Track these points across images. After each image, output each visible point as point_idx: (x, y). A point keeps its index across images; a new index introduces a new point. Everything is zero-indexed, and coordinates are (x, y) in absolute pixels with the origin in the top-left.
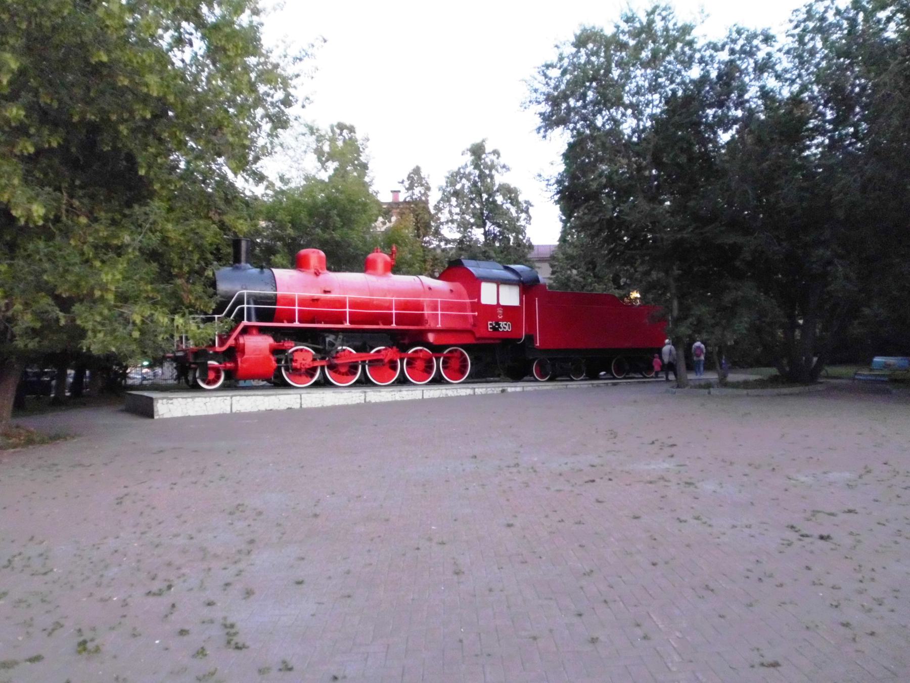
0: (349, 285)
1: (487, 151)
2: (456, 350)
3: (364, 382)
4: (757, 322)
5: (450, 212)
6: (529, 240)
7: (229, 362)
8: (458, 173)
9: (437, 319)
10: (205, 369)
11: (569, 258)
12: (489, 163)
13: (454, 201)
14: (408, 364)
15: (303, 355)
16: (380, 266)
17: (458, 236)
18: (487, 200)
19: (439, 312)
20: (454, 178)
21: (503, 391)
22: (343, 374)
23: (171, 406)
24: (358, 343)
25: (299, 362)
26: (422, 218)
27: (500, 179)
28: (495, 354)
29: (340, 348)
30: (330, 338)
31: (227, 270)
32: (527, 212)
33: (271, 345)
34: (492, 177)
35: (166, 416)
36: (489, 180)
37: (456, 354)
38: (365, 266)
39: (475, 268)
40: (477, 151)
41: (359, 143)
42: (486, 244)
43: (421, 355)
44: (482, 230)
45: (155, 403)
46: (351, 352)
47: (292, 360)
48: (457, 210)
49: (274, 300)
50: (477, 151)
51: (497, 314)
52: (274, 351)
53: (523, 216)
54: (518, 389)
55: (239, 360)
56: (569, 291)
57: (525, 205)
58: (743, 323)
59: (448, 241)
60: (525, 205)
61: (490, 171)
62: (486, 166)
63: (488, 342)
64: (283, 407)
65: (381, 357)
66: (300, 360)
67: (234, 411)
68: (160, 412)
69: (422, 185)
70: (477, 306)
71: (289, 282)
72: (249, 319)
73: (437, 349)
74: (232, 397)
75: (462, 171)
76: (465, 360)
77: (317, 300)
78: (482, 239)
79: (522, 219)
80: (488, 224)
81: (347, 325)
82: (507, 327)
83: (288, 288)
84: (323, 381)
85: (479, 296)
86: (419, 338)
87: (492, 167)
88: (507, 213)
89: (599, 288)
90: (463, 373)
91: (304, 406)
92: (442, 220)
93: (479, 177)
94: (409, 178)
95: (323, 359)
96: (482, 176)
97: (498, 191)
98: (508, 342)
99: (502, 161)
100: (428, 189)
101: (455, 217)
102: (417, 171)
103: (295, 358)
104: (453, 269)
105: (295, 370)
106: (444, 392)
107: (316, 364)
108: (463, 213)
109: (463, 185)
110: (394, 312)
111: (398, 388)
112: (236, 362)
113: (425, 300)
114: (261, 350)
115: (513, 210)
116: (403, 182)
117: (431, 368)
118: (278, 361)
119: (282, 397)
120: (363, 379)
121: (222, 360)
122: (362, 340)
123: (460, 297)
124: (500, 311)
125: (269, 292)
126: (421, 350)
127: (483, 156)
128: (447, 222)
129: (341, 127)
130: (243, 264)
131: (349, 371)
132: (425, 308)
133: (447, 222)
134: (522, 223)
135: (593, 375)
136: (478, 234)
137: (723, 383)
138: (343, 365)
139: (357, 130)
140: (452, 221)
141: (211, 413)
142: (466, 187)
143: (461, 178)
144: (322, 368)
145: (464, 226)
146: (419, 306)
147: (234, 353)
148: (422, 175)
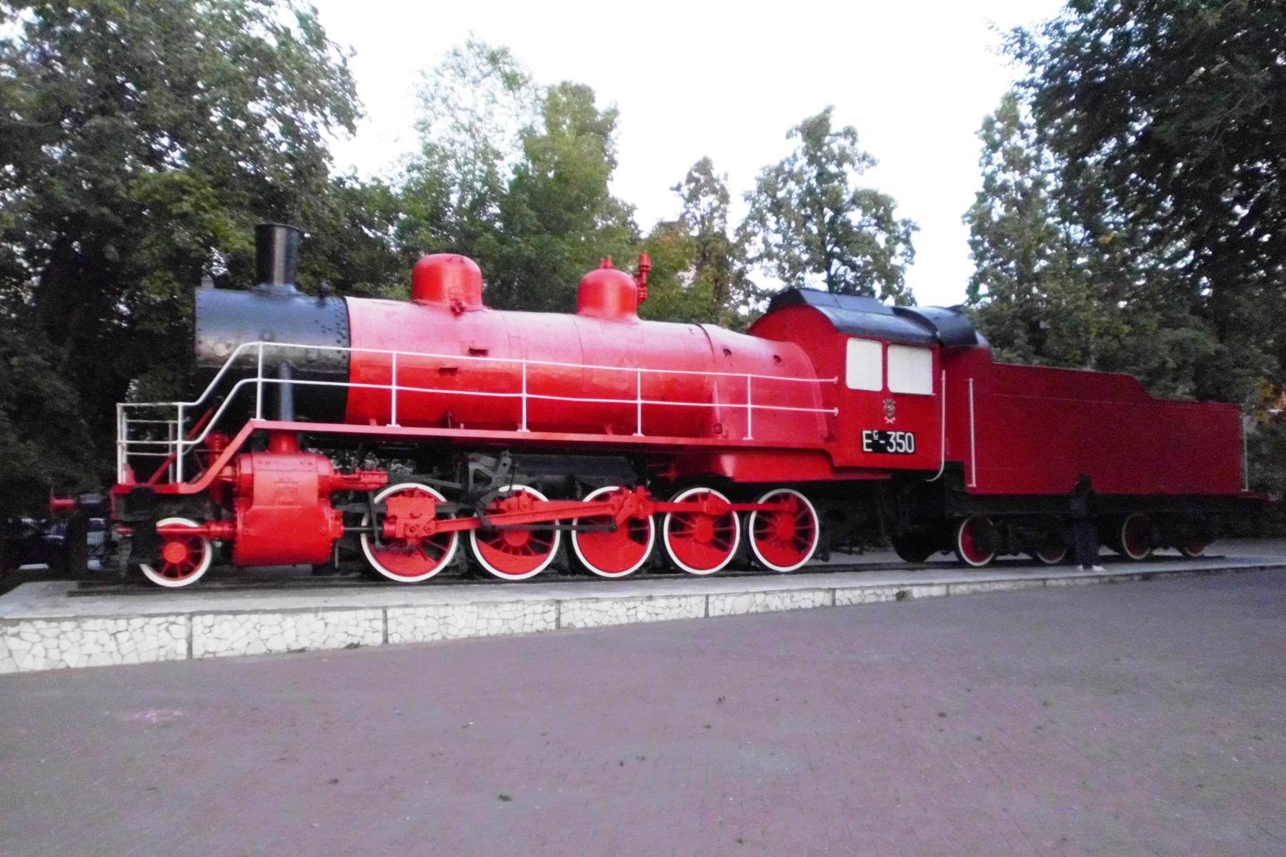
0: (531, 342)
1: (833, 130)
2: (786, 496)
3: (569, 570)
5: (765, 241)
8: (779, 170)
10: (150, 545)
12: (837, 151)
13: (771, 220)
14: (672, 529)
16: (611, 297)
17: (778, 285)
18: (832, 221)
19: (749, 406)
21: (901, 596)
22: (515, 552)
23: (13, 643)
24: (557, 478)
26: (713, 249)
27: (856, 180)
28: (871, 498)
30: (479, 464)
32: (907, 241)
33: (323, 480)
34: (841, 176)
37: (786, 506)
38: (572, 299)
43: (705, 507)
46: (535, 499)
47: (382, 518)
48: (778, 239)
49: (345, 369)
50: (815, 132)
51: (884, 413)
52: (331, 492)
53: (900, 248)
54: (937, 591)
55: (240, 515)
57: (902, 229)
60: (902, 229)
62: (831, 157)
64: (337, 641)
65: (609, 511)
66: (403, 518)
67: (198, 652)
69: (714, 191)
70: (838, 393)
71: (383, 330)
72: (270, 413)
73: (742, 493)
74: (192, 615)
75: (787, 168)
76: (808, 519)
77: (453, 371)
80: (836, 263)
81: (523, 432)
82: (905, 444)
83: (381, 342)
85: (841, 370)
86: (699, 465)
87: (842, 159)
90: (803, 548)
91: (394, 639)
92: (750, 255)
94: (690, 179)
96: (822, 176)
98: (907, 480)
99: (861, 147)
100: (724, 198)
102: (704, 167)
103: (391, 512)
105: (388, 540)
106: (760, 599)
107: (444, 527)
110: (639, 402)
112: (233, 522)
114: (294, 491)
116: (678, 188)
117: (729, 536)
120: (565, 563)
122: (564, 469)
123: (798, 370)
125: (330, 348)
126: (705, 496)
127: (827, 139)
128: (760, 258)
130: (278, 283)
131: (530, 542)
132: (716, 396)
133: (760, 258)
134: (896, 261)
138: (514, 530)
140: (769, 255)
141: (132, 659)
143: (785, 181)
144: (464, 536)
146: (699, 390)
147: (231, 494)
148: (715, 174)
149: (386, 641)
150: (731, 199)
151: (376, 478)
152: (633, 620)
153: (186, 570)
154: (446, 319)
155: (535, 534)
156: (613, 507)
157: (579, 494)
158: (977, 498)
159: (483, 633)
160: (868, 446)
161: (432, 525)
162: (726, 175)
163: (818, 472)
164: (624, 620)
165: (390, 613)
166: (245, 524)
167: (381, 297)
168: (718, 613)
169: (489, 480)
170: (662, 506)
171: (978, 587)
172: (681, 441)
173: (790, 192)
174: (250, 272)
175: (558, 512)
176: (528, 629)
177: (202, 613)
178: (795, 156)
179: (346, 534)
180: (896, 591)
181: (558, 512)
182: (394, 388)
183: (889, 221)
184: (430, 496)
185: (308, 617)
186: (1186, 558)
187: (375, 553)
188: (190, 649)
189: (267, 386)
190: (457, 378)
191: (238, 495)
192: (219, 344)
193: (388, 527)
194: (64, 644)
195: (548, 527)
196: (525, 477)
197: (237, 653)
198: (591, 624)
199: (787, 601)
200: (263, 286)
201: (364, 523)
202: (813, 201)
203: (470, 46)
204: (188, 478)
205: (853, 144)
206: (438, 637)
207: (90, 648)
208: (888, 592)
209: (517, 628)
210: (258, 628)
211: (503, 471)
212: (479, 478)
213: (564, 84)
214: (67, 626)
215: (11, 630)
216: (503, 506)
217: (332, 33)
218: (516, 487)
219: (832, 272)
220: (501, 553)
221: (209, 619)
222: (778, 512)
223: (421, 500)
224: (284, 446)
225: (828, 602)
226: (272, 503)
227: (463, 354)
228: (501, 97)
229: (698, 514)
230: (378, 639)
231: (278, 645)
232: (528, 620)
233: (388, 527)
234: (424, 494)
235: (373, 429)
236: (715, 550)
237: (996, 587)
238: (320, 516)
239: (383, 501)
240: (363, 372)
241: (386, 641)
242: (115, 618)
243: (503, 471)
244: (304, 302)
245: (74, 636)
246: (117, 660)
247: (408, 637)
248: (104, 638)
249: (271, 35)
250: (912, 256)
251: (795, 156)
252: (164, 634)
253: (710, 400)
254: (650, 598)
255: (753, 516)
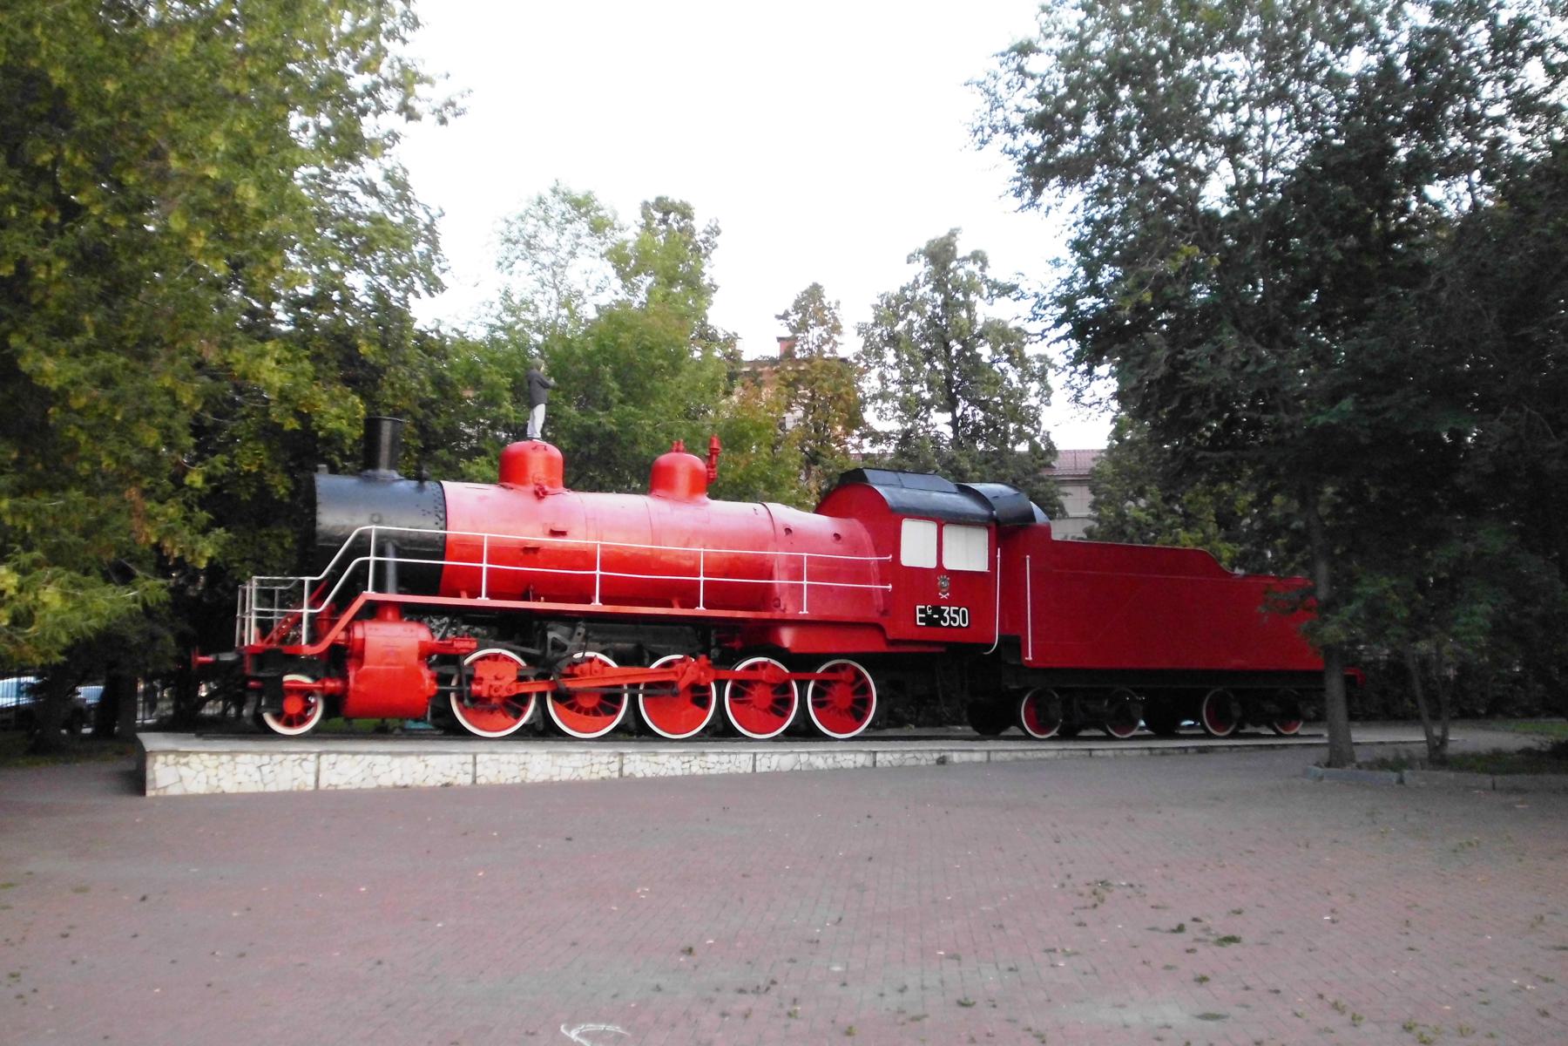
0: (610, 520)
1: (959, 255)
2: (844, 666)
3: (634, 731)
4: (1512, 616)
5: (882, 377)
6: (1046, 438)
7: (331, 679)
8: (901, 298)
9: (799, 600)
10: (276, 695)
11: (1134, 475)
13: (890, 356)
15: (500, 667)
16: (683, 480)
19: (805, 582)
20: (894, 308)
21: (942, 761)
22: (587, 713)
23: (184, 770)
24: (626, 646)
25: (486, 683)
27: (986, 310)
28: (928, 674)
29: (578, 656)
31: (346, 482)
32: (1042, 378)
33: (422, 644)
34: (969, 307)
35: (175, 791)
36: (964, 314)
37: (843, 675)
38: (651, 479)
39: (890, 491)
40: (940, 254)
41: (699, 237)
42: (955, 443)
43: (763, 675)
44: (948, 417)
45: (149, 763)
46: (606, 665)
47: (471, 679)
49: (439, 547)
50: (940, 254)
53: (1035, 386)
54: (977, 757)
55: (352, 674)
56: (1124, 543)
57: (1038, 365)
58: (1479, 612)
59: (877, 438)
60: (1038, 365)
61: (966, 295)
63: (914, 649)
64: (435, 780)
65: (672, 678)
67: (323, 784)
68: (160, 784)
69: (823, 323)
71: (476, 511)
72: (380, 586)
73: (801, 663)
74: (319, 754)
75: (908, 294)
77: (535, 550)
78: (948, 432)
79: (1032, 393)
80: (962, 404)
81: (596, 605)
82: (959, 620)
84: (541, 726)
85: (896, 550)
86: (760, 637)
87: (970, 287)
88: (998, 381)
89: (1187, 539)
90: (860, 718)
93: (945, 305)
94: (798, 307)
95: (543, 677)
96: (949, 305)
97: (980, 336)
98: (961, 655)
100: (836, 329)
101: (893, 388)
102: (815, 292)
103: (478, 674)
104: (846, 492)
105: (477, 699)
106: (804, 758)
107: (525, 689)
108: (910, 382)
109: (911, 323)
110: (702, 578)
111: (316, 747)
112: (345, 679)
113: (778, 555)
114: (398, 654)
115: (1013, 375)
116: (785, 316)
117: (790, 702)
118: (443, 679)
119: (433, 760)
120: (632, 725)
121: (319, 674)
123: (856, 548)
124: (944, 583)
125: (429, 529)
126: (764, 665)
127: (953, 265)
128: (874, 398)
129: (665, 207)
130: (383, 471)
131: (600, 705)
135: (1164, 728)
136: (940, 422)
137: (1438, 757)
138: (586, 693)
139: (697, 213)
141: (272, 788)
142: (916, 326)
143: (907, 309)
145: (911, 407)
146: (763, 569)
147: (342, 657)
149: (474, 782)
150: (843, 330)
151: (467, 644)
152: (687, 772)
153: (301, 719)
154: (532, 500)
155: (605, 697)
156: (676, 673)
157: (646, 661)
158: (1032, 670)
159: (556, 779)
160: (921, 620)
161: (514, 686)
162: (838, 303)
163: (874, 645)
164: (679, 772)
165: (479, 758)
166: (356, 681)
167: (471, 481)
168: (764, 769)
169: (564, 648)
170: (723, 674)
171: (1020, 755)
172: (740, 614)
173: (911, 323)
174: (365, 458)
175: (627, 677)
176: (594, 777)
177: (328, 753)
178: (916, 281)
179: (439, 692)
180: (936, 756)
181: (627, 677)
182: (485, 565)
183: (1022, 356)
184: (512, 660)
185: (412, 759)
186: (1279, 735)
187: (463, 710)
188: (317, 780)
189: (378, 564)
190: (539, 556)
191: (350, 656)
192: (329, 519)
193: (474, 687)
194: (222, 773)
195: (617, 691)
196: (597, 644)
197: (353, 787)
198: (649, 774)
199: (830, 761)
200: (370, 472)
201: (454, 683)
202: (939, 335)
203: (555, 191)
204: (313, 640)
205: (982, 269)
206: (518, 780)
207: (241, 777)
208: (928, 756)
209: (585, 775)
210: (371, 766)
211: (577, 640)
212: (557, 646)
213: (659, 200)
214: (225, 758)
215: (183, 760)
216: (577, 670)
217: (418, 191)
218: (588, 654)
219: (959, 413)
220: (574, 714)
221: (333, 757)
222: (836, 682)
223: (505, 664)
224: (390, 615)
225: (869, 763)
226: (379, 664)
227: (545, 535)
228: (585, 240)
229: (757, 682)
230: (468, 780)
231: (386, 781)
232: (595, 768)
233: (474, 687)
234: (506, 658)
235: (464, 601)
236: (773, 716)
237: (1039, 755)
238: (420, 676)
239: (471, 664)
240: (457, 551)
241: (474, 782)
242: (261, 754)
243: (577, 640)
244: (408, 486)
245: (230, 767)
246: (260, 788)
247: (493, 780)
248: (252, 769)
249: (357, 188)
250: (1049, 395)
251: (916, 281)
252: (297, 769)
253: (771, 577)
254: (703, 754)
255: (811, 685)
